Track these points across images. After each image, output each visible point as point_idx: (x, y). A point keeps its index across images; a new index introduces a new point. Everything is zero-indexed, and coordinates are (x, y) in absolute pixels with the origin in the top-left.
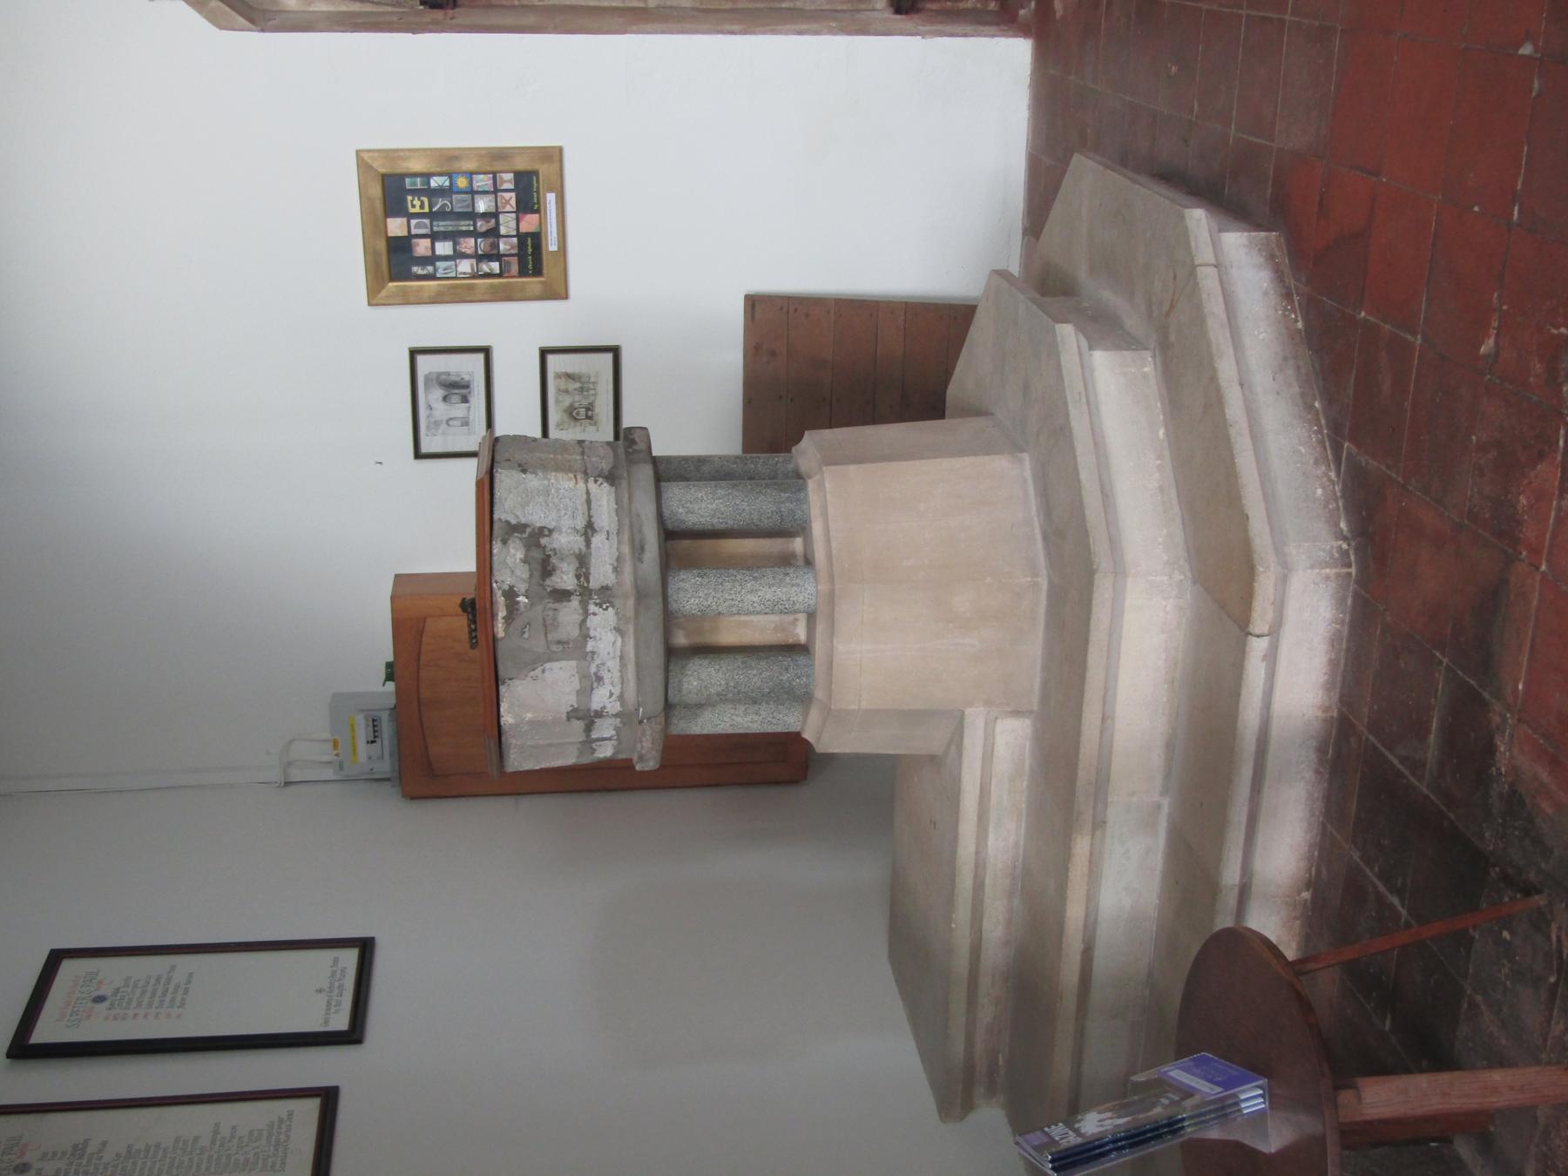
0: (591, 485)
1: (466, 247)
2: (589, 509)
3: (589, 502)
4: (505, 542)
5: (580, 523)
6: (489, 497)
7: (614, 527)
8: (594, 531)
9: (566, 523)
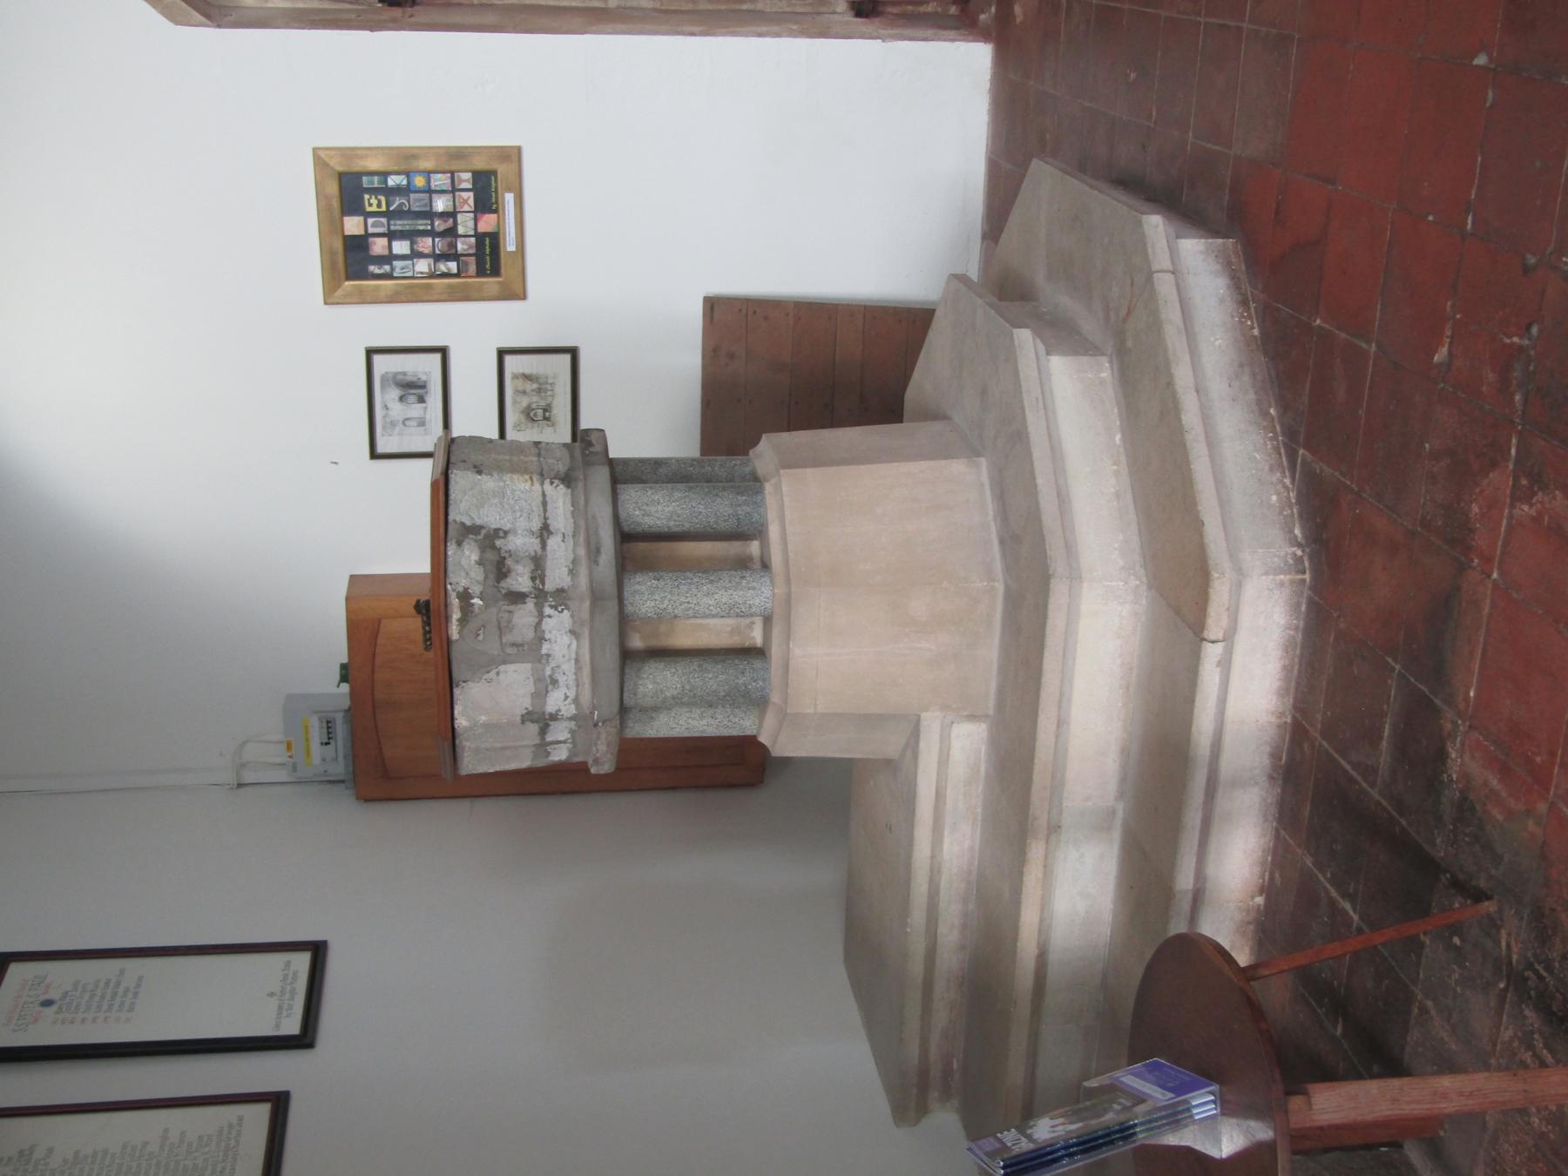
0: (548, 487)
2: (545, 511)
4: (459, 544)
5: (536, 525)
8: (550, 533)
9: (522, 524)
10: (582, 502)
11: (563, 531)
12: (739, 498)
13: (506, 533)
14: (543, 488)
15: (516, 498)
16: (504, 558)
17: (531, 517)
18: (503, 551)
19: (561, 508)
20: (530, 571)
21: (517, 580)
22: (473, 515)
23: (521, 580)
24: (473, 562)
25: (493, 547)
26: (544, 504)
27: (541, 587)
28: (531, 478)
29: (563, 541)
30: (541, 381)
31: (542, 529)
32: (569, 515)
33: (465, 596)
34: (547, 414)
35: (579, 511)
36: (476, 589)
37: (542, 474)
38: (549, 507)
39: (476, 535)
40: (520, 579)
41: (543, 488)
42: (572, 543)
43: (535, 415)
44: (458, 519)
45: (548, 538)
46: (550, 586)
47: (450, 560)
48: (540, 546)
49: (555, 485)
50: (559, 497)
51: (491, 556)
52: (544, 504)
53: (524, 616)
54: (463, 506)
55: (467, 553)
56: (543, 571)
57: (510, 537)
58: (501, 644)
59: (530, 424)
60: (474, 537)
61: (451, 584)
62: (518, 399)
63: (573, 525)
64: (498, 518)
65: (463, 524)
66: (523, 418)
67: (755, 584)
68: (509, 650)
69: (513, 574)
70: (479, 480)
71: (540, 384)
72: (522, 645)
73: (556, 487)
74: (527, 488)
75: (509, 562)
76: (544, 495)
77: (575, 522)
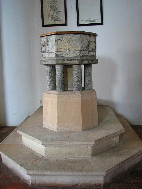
0: (55, 53)
1: (77, 38)
2: (52, 52)
3: (53, 52)
4: (46, 38)
5: (50, 51)
6: (84, 72)
7: (50, 57)
8: (49, 53)
9: (50, 49)
37: (57, 52)
46: (43, 54)
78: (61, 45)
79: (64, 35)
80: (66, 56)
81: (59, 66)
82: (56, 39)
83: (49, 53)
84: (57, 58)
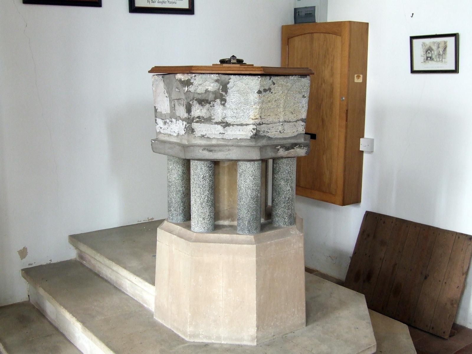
0: (251, 127)
2: (237, 125)
4: (217, 81)
5: (229, 120)
8: (224, 127)
9: (229, 113)
10: (243, 144)
11: (226, 133)
12: (247, 222)
13: (224, 105)
14: (251, 124)
15: (244, 110)
16: (210, 103)
17: (234, 118)
18: (213, 103)
19: (239, 133)
20: (203, 116)
21: (198, 109)
22: (234, 88)
23: (197, 111)
24: (207, 87)
25: (216, 98)
26: (242, 125)
27: (194, 121)
28: (256, 119)
29: (220, 133)
30: (444, 55)
31: (227, 123)
32: (235, 137)
33: (188, 83)
34: (429, 59)
35: (237, 143)
36: (192, 89)
37: (260, 124)
38: (239, 127)
39: (222, 89)
40: (198, 111)
41: (251, 124)
42: (219, 138)
43: (429, 53)
44: (231, 80)
45: (221, 126)
46: (195, 125)
47: (208, 75)
48: (217, 121)
49: (253, 130)
50: (247, 132)
51: (211, 97)
52: (242, 125)
53: (182, 112)
54: (239, 83)
55: (212, 85)
56: (203, 122)
57: (221, 107)
58: (174, 100)
59: (425, 51)
60: (220, 89)
61: (195, 76)
62: (436, 44)
63: (229, 139)
64: (233, 101)
65: (228, 83)
66: (427, 47)
67: (200, 224)
68: (173, 103)
69: (201, 107)
70: (254, 92)
71: (442, 55)
72: (175, 110)
73: (252, 131)
74: (251, 116)
75: (208, 106)
76: (247, 125)
77: (231, 139)
78: (270, 104)
79: (278, 78)
80: (276, 137)
81: (258, 162)
82: (262, 89)
83: (226, 125)
84: (256, 142)
